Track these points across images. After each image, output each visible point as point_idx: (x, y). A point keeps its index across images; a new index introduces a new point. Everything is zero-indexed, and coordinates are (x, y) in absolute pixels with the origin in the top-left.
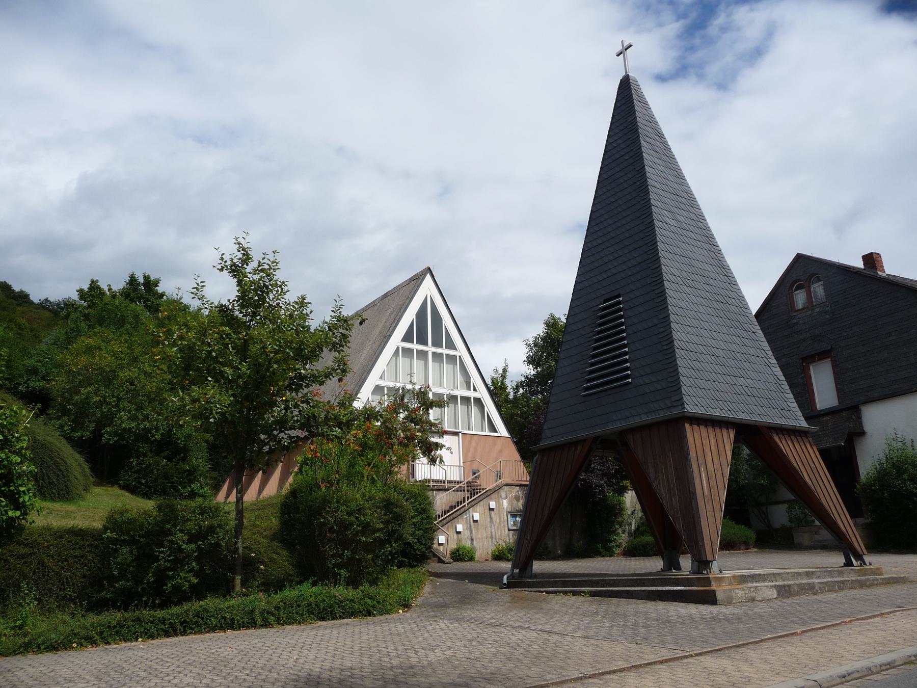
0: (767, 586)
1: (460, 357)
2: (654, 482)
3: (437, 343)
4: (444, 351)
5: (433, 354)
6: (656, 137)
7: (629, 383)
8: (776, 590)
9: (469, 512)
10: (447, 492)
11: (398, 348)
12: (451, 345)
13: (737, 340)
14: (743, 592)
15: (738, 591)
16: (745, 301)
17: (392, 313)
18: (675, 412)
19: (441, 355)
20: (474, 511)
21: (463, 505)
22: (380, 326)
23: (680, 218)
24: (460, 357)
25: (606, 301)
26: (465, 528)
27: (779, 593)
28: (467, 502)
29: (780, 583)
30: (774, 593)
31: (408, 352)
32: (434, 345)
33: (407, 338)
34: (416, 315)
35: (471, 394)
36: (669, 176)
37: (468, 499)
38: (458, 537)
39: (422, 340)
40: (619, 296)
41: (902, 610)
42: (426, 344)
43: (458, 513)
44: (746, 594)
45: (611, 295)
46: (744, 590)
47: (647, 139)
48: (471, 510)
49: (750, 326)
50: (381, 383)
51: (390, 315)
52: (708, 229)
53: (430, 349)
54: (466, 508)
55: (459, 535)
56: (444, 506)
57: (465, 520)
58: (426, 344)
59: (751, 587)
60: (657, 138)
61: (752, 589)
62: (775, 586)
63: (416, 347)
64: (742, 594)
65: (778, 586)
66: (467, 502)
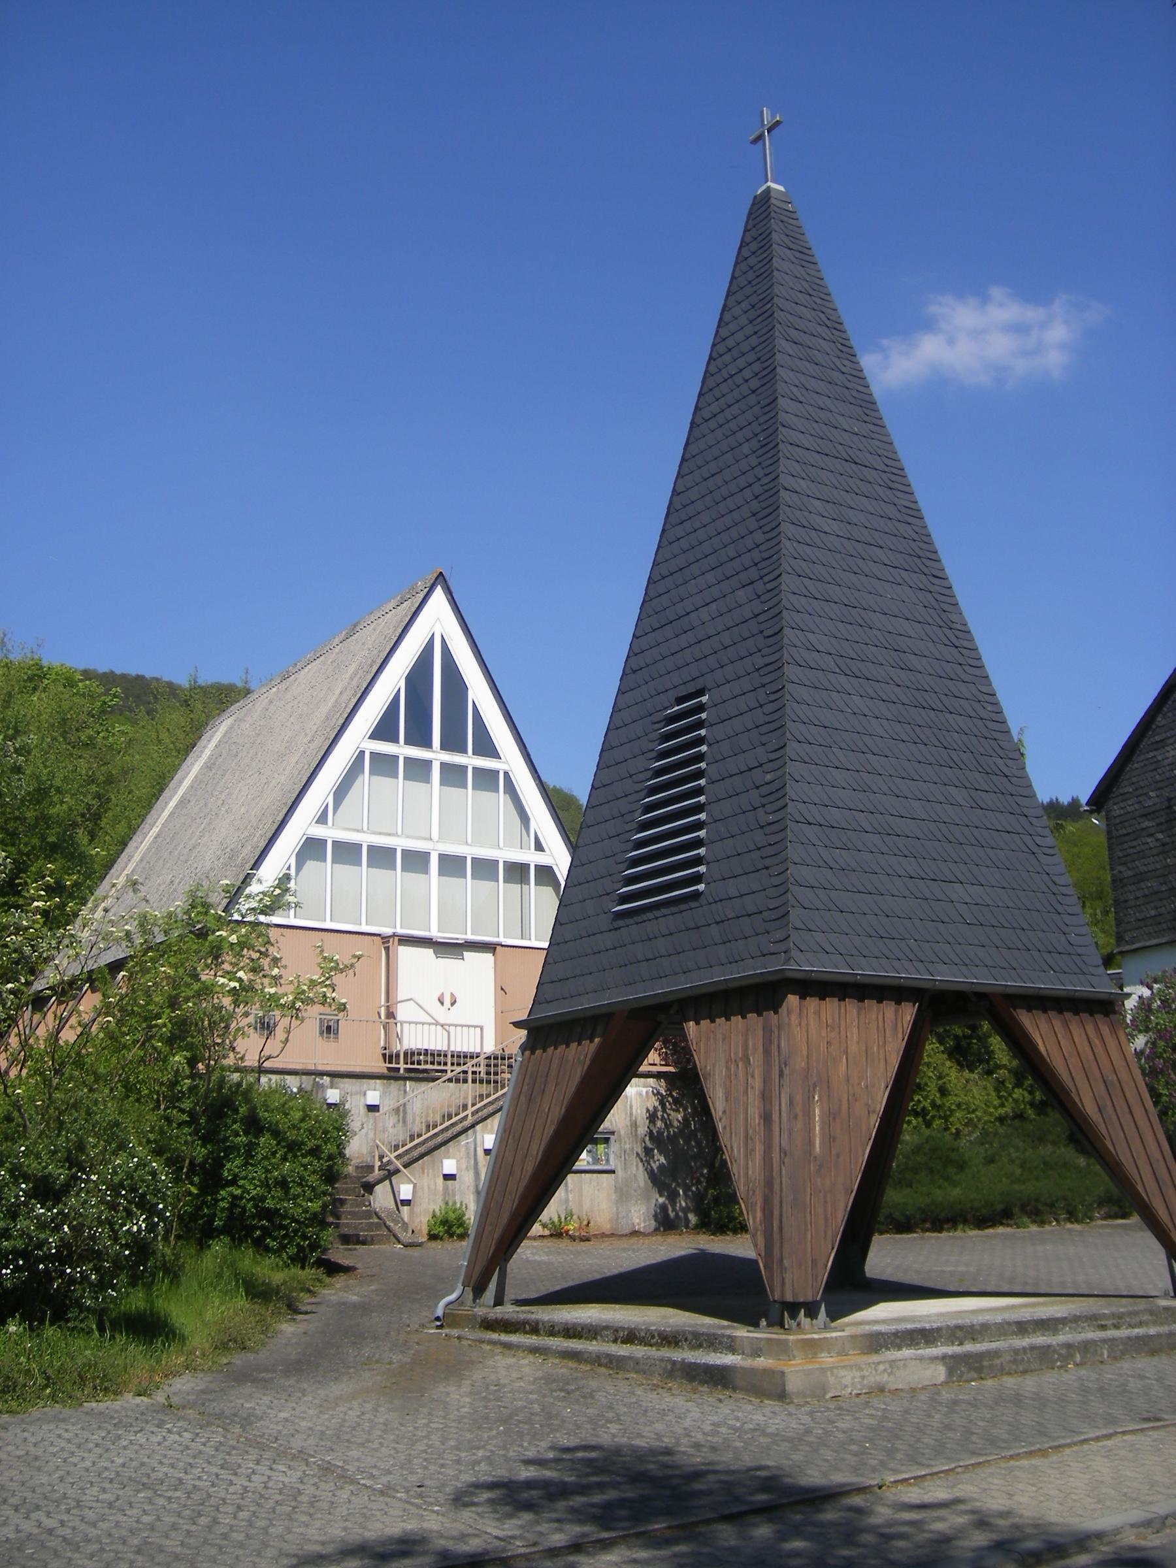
0: (921, 1359)
1: (506, 774)
2: (720, 1120)
3: (453, 742)
4: (470, 760)
5: (444, 765)
6: (820, 329)
7: (696, 895)
8: (945, 1364)
9: (475, 1133)
10: (432, 1084)
11: (362, 753)
12: (486, 747)
13: (958, 795)
14: (858, 1374)
15: (842, 1372)
16: (997, 704)
17: (355, 674)
18: (771, 966)
19: (463, 769)
20: (484, 1130)
21: (462, 1115)
22: (332, 700)
23: (852, 515)
24: (506, 774)
25: (680, 700)
26: (464, 1166)
27: (950, 1372)
28: (470, 1110)
29: (955, 1349)
30: (939, 1373)
31: (384, 765)
32: (445, 746)
33: (385, 730)
34: (407, 678)
35: (532, 858)
36: (840, 418)
37: (473, 1105)
38: (446, 1189)
39: (419, 736)
40: (701, 693)
41: (1164, 1426)
42: (427, 743)
43: (449, 1134)
44: (863, 1377)
45: (691, 688)
46: (860, 1369)
47: (794, 334)
48: (478, 1127)
49: (999, 761)
50: (319, 832)
51: (351, 679)
52: (925, 538)
53: (437, 756)
54: (467, 1123)
55: (450, 1182)
56: (427, 1115)
57: (463, 1150)
58: (427, 743)
59: (879, 1363)
60: (823, 331)
61: (881, 1367)
62: (944, 1358)
63: (402, 750)
64: (853, 1378)
65: (952, 1357)
66: (470, 1110)
